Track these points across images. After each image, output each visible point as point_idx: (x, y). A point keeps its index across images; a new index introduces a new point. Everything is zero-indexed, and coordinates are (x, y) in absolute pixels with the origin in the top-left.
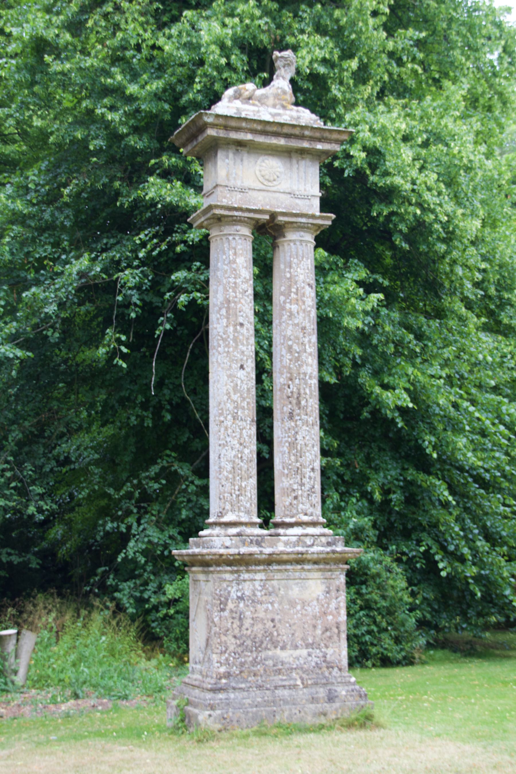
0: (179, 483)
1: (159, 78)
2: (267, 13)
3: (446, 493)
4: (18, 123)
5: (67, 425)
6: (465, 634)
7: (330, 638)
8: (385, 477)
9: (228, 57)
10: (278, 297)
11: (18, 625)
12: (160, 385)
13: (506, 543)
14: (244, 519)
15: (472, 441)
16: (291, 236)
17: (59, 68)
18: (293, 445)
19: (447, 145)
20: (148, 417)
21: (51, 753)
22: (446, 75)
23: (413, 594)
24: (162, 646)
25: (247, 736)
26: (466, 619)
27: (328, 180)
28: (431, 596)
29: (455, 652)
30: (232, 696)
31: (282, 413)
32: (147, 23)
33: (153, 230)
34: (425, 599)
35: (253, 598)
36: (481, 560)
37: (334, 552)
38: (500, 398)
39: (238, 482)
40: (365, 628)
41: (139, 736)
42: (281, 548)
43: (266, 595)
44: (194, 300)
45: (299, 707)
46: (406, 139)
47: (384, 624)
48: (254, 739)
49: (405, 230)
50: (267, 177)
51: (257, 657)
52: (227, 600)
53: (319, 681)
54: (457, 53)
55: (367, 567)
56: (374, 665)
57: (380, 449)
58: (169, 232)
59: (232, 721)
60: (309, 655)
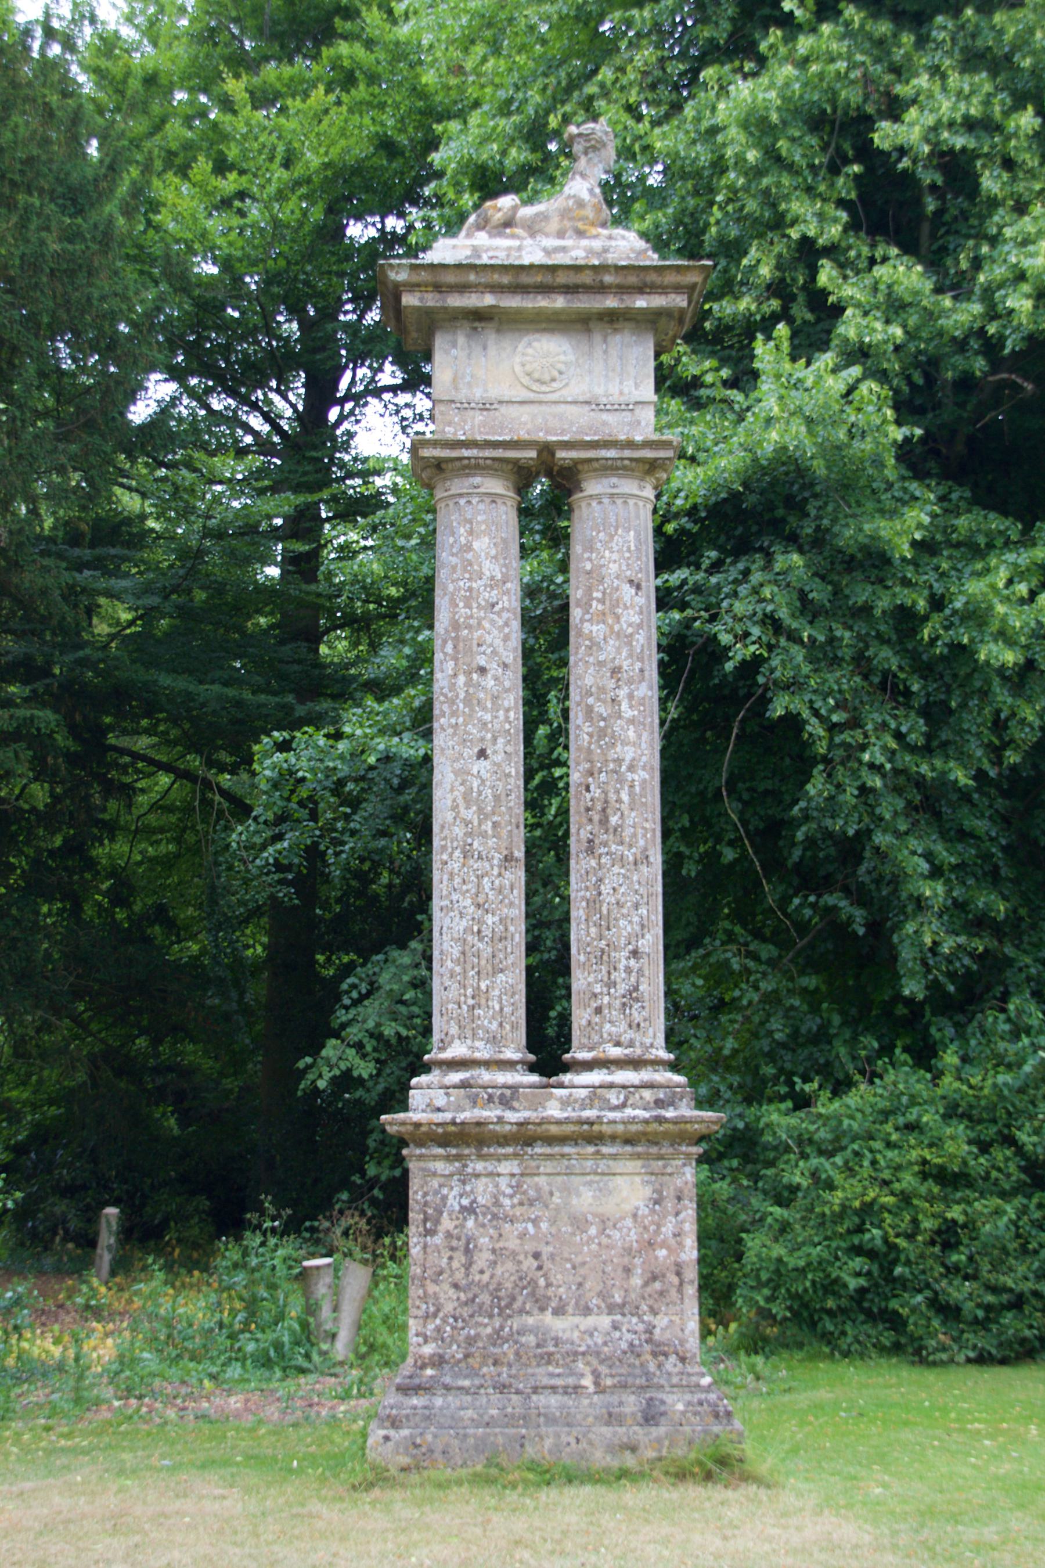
7: (662, 1293)
14: (484, 1052)
16: (593, 487)
20: (690, 858)
35: (495, 1210)
39: (472, 982)
42: (554, 1111)
43: (521, 1204)
45: (575, 1432)
50: (536, 375)
51: (502, 1328)
52: (441, 1213)
53: (630, 1380)
59: (432, 1451)
60: (616, 1327)
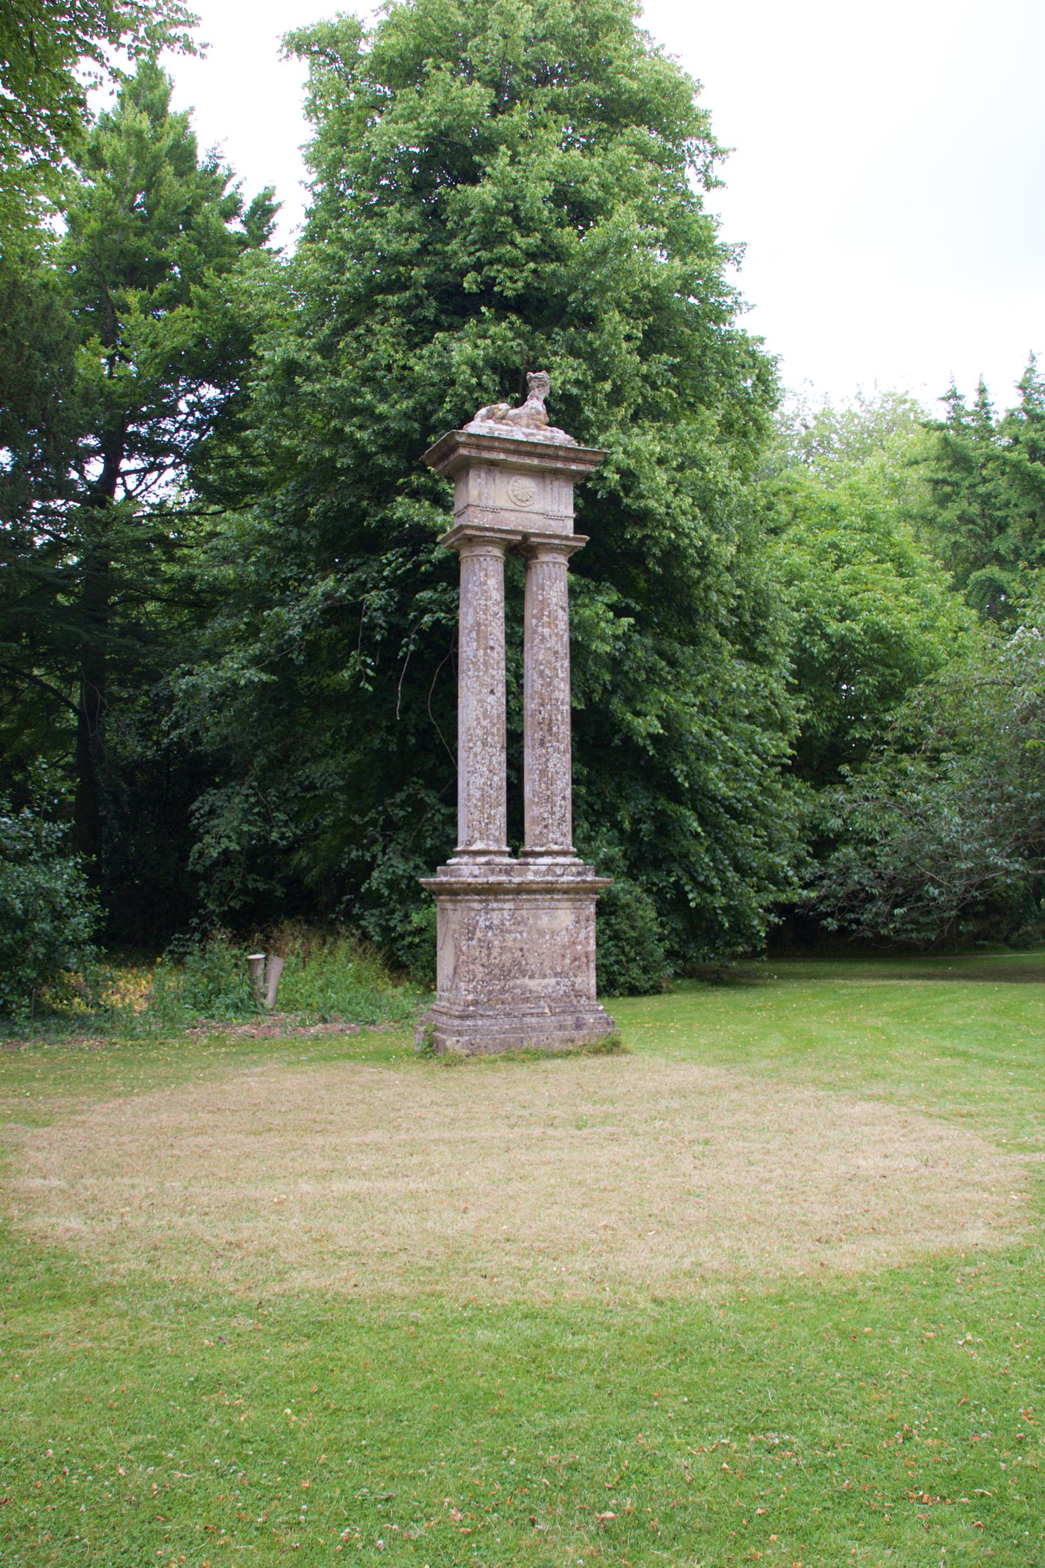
0: (425, 811)
1: (409, 397)
2: (519, 335)
3: (695, 824)
4: (267, 443)
5: (312, 750)
6: (713, 963)
7: (579, 967)
8: (636, 806)
9: (479, 378)
10: (530, 621)
11: (265, 950)
12: (405, 710)
13: (756, 874)
14: (493, 847)
15: (725, 771)
16: (544, 558)
17: (309, 389)
18: (543, 772)
19: (702, 469)
21: (303, 1072)
22: (701, 400)
23: (662, 925)
24: (408, 974)
25: (495, 1061)
26: (714, 948)
27: (580, 501)
28: (679, 926)
29: (702, 981)
30: (480, 1023)
31: (533, 739)
32: (399, 344)
33: (401, 551)
34: (673, 929)
36: (731, 891)
37: (584, 882)
38: (753, 727)
40: (613, 958)
41: (387, 1059)
42: (530, 877)
44: (438, 620)
46: (661, 461)
47: (633, 954)
48: (501, 1064)
49: (658, 553)
54: (711, 379)
55: (617, 897)
56: (621, 994)
57: (632, 778)
58: (416, 552)
60: (558, 984)
